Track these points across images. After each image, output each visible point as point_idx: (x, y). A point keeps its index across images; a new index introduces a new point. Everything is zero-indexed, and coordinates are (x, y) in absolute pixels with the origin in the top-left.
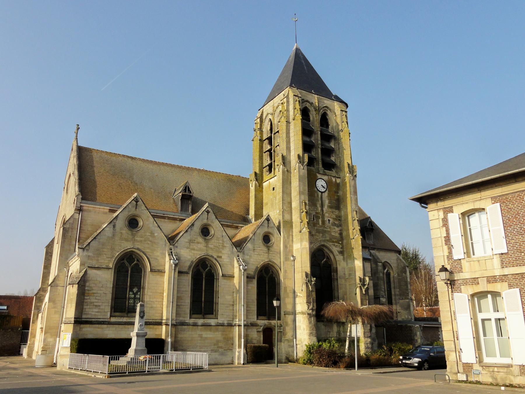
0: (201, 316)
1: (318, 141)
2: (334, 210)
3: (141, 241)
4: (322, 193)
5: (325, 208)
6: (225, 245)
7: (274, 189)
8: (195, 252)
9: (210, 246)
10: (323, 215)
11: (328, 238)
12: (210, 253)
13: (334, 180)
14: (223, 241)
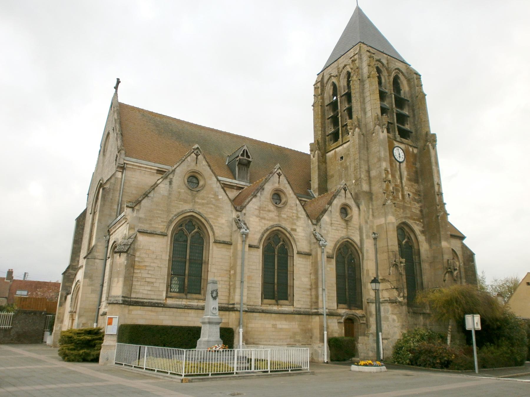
0: (273, 301)
1: (392, 105)
2: (413, 183)
3: (203, 204)
4: (400, 163)
5: (404, 180)
6: (300, 216)
7: (342, 158)
8: (266, 222)
9: (283, 216)
10: (402, 188)
11: (409, 215)
12: (284, 224)
13: (411, 149)
14: (297, 210)
